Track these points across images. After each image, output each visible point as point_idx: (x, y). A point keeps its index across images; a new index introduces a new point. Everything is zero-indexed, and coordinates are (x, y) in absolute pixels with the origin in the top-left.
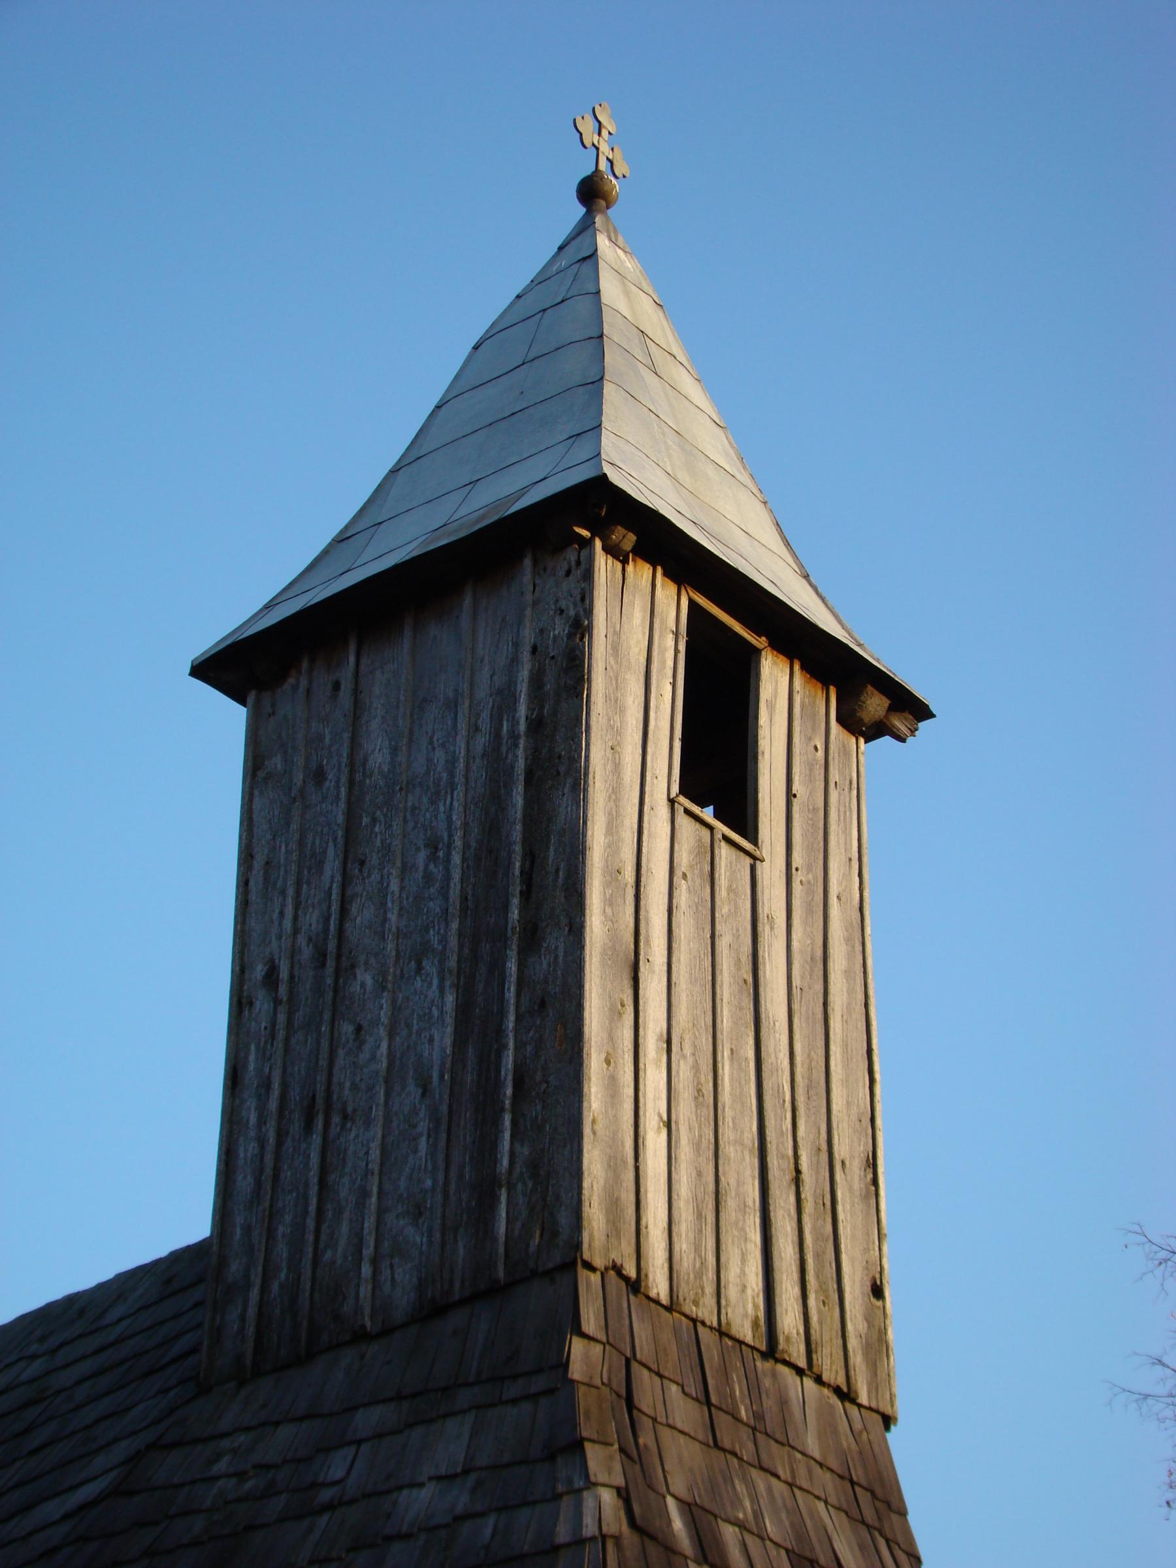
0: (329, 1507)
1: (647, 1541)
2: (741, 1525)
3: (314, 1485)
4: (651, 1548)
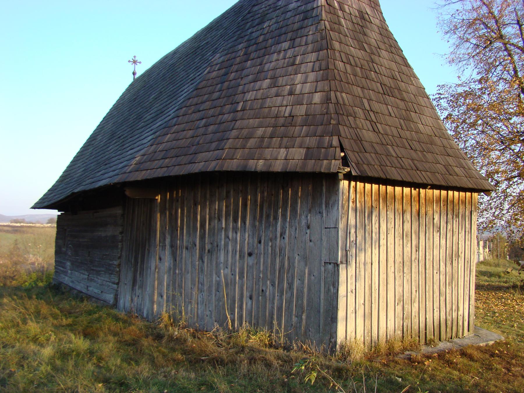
0: (279, 9)
1: (330, 7)
2: (349, 6)
3: (277, 6)
4: (331, 8)
